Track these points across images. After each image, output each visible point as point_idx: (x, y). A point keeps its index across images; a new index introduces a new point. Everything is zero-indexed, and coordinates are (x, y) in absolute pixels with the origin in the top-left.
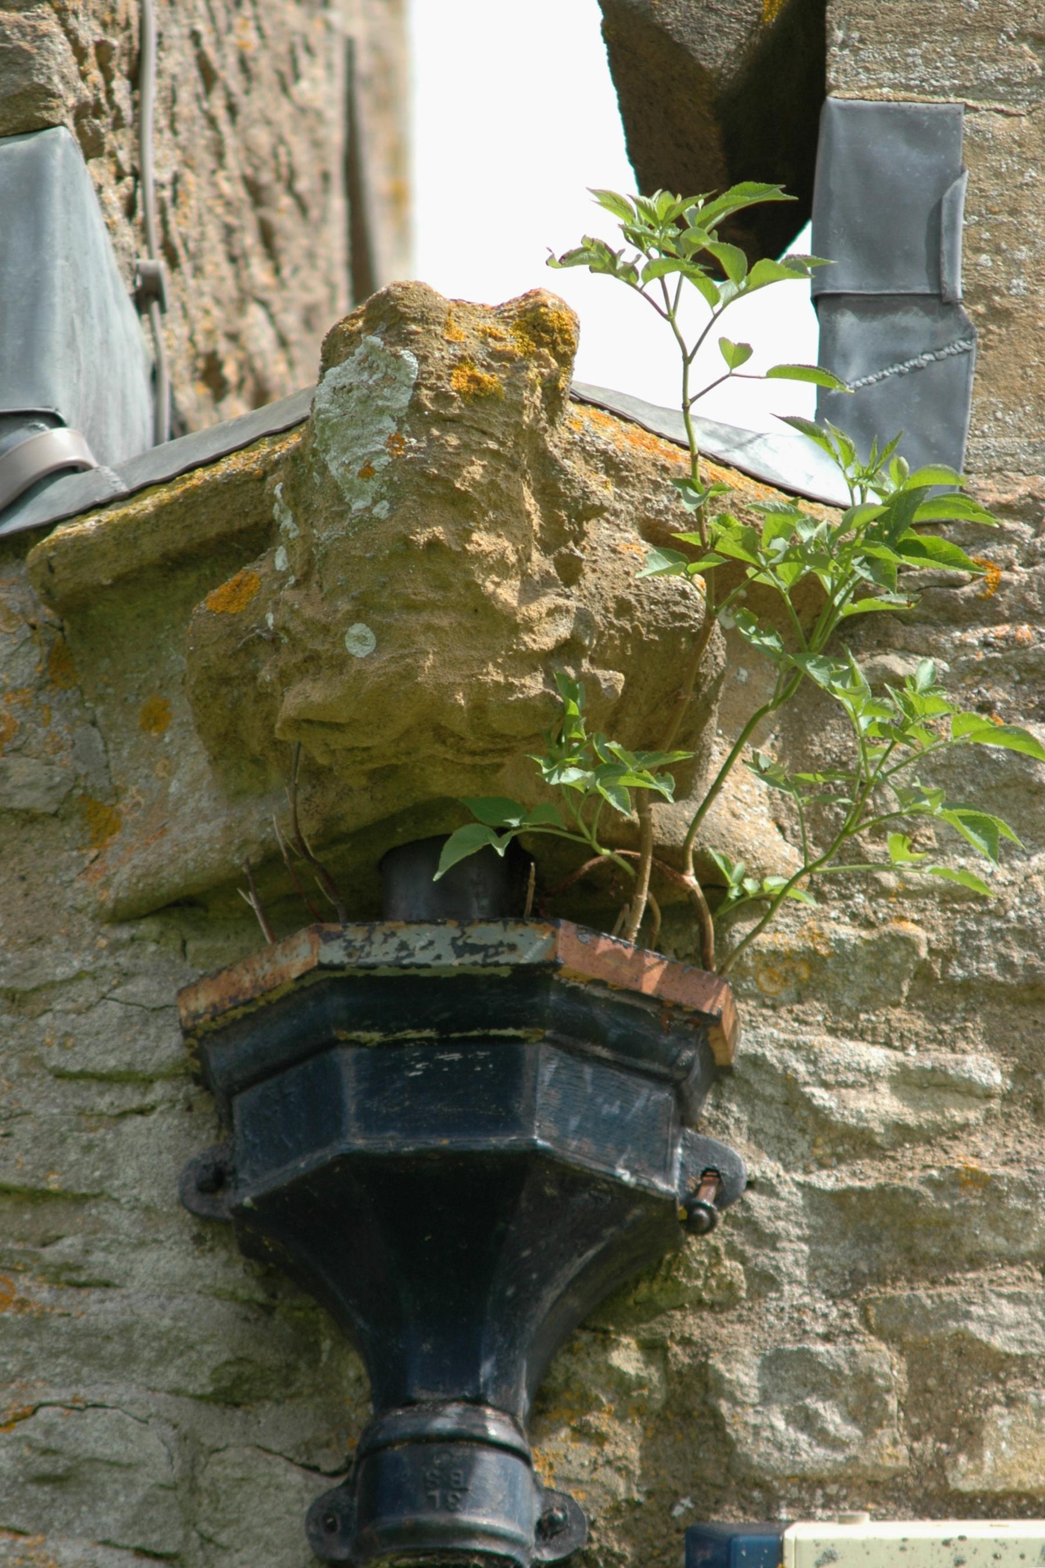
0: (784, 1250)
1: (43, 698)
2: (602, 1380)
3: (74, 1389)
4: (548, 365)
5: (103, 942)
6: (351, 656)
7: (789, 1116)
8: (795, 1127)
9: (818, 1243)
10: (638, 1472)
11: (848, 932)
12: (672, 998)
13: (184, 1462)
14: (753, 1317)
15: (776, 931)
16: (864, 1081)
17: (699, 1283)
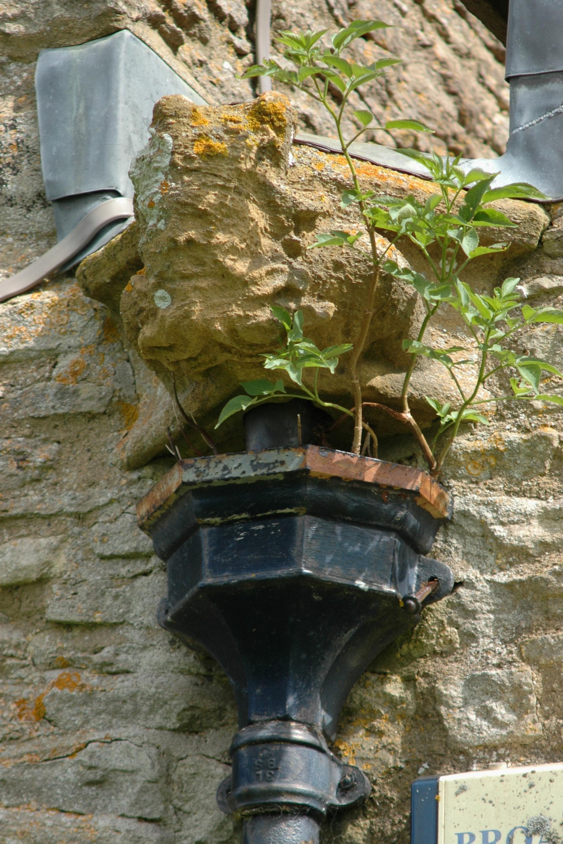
0: (480, 619)
1: (101, 349)
2: (381, 701)
3: (107, 732)
4: (268, 134)
5: (124, 481)
6: (158, 308)
7: (484, 543)
8: (486, 549)
9: (499, 613)
10: (400, 751)
11: (515, 436)
12: (385, 483)
13: (162, 767)
14: (463, 658)
15: (477, 439)
16: (524, 519)
17: (433, 642)
